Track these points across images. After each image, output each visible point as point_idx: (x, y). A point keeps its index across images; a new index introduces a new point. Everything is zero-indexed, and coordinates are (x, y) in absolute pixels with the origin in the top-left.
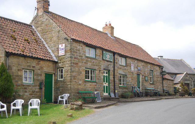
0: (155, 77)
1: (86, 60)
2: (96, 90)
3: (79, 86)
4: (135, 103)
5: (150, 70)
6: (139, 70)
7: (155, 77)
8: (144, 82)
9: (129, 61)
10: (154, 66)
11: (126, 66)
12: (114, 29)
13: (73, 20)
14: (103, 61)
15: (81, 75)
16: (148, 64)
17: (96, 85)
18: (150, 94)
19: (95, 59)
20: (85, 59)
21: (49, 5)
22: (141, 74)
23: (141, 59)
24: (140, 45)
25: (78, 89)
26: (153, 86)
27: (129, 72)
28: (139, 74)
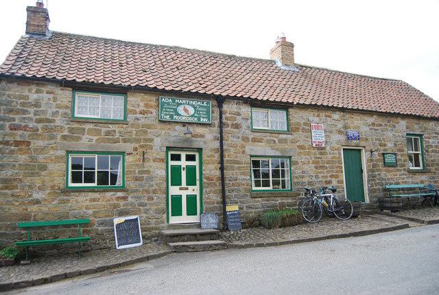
0: (433, 151)
1: (71, 130)
2: (121, 214)
3: (33, 209)
4: (283, 250)
5: (407, 134)
6: (349, 138)
7: (433, 151)
8: (379, 170)
9: (298, 116)
10: (422, 122)
11: (290, 131)
12: (293, 47)
13: (375, 76)
14: (160, 126)
15: (43, 173)
16: (399, 120)
17: (125, 198)
18: (389, 205)
19: (124, 122)
20: (66, 126)
21: (47, 18)
22: (364, 147)
23: (373, 107)
24: (407, 81)
25: (26, 217)
26: (424, 177)
27: (301, 147)
28: (360, 150)
